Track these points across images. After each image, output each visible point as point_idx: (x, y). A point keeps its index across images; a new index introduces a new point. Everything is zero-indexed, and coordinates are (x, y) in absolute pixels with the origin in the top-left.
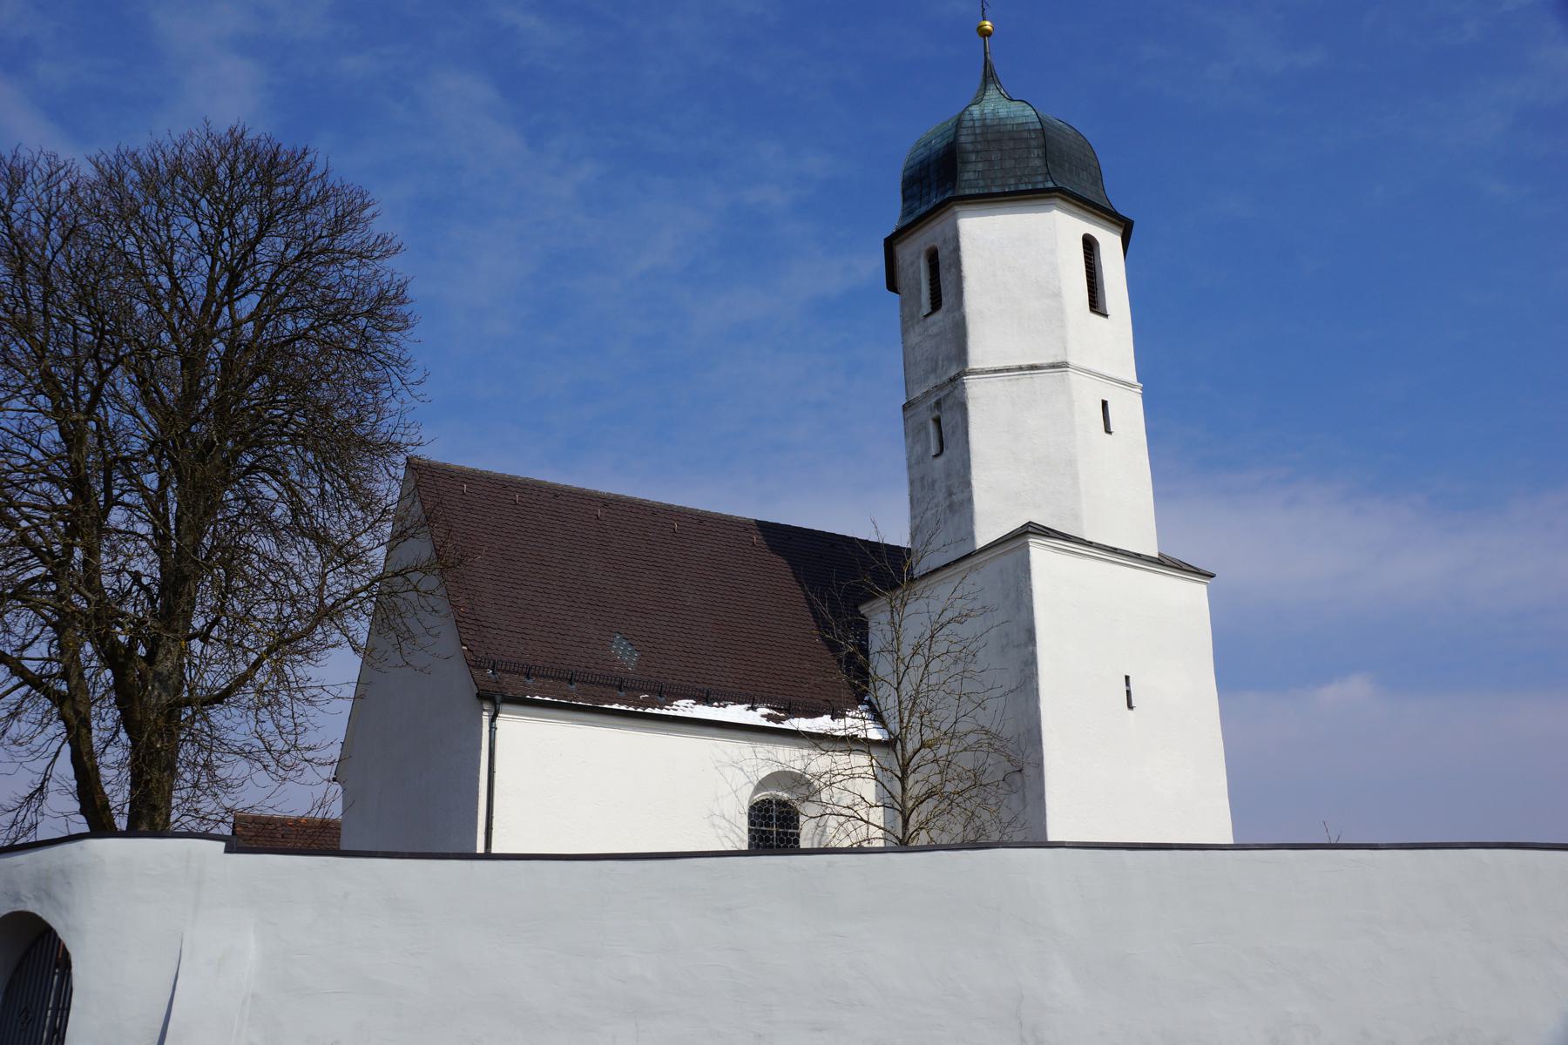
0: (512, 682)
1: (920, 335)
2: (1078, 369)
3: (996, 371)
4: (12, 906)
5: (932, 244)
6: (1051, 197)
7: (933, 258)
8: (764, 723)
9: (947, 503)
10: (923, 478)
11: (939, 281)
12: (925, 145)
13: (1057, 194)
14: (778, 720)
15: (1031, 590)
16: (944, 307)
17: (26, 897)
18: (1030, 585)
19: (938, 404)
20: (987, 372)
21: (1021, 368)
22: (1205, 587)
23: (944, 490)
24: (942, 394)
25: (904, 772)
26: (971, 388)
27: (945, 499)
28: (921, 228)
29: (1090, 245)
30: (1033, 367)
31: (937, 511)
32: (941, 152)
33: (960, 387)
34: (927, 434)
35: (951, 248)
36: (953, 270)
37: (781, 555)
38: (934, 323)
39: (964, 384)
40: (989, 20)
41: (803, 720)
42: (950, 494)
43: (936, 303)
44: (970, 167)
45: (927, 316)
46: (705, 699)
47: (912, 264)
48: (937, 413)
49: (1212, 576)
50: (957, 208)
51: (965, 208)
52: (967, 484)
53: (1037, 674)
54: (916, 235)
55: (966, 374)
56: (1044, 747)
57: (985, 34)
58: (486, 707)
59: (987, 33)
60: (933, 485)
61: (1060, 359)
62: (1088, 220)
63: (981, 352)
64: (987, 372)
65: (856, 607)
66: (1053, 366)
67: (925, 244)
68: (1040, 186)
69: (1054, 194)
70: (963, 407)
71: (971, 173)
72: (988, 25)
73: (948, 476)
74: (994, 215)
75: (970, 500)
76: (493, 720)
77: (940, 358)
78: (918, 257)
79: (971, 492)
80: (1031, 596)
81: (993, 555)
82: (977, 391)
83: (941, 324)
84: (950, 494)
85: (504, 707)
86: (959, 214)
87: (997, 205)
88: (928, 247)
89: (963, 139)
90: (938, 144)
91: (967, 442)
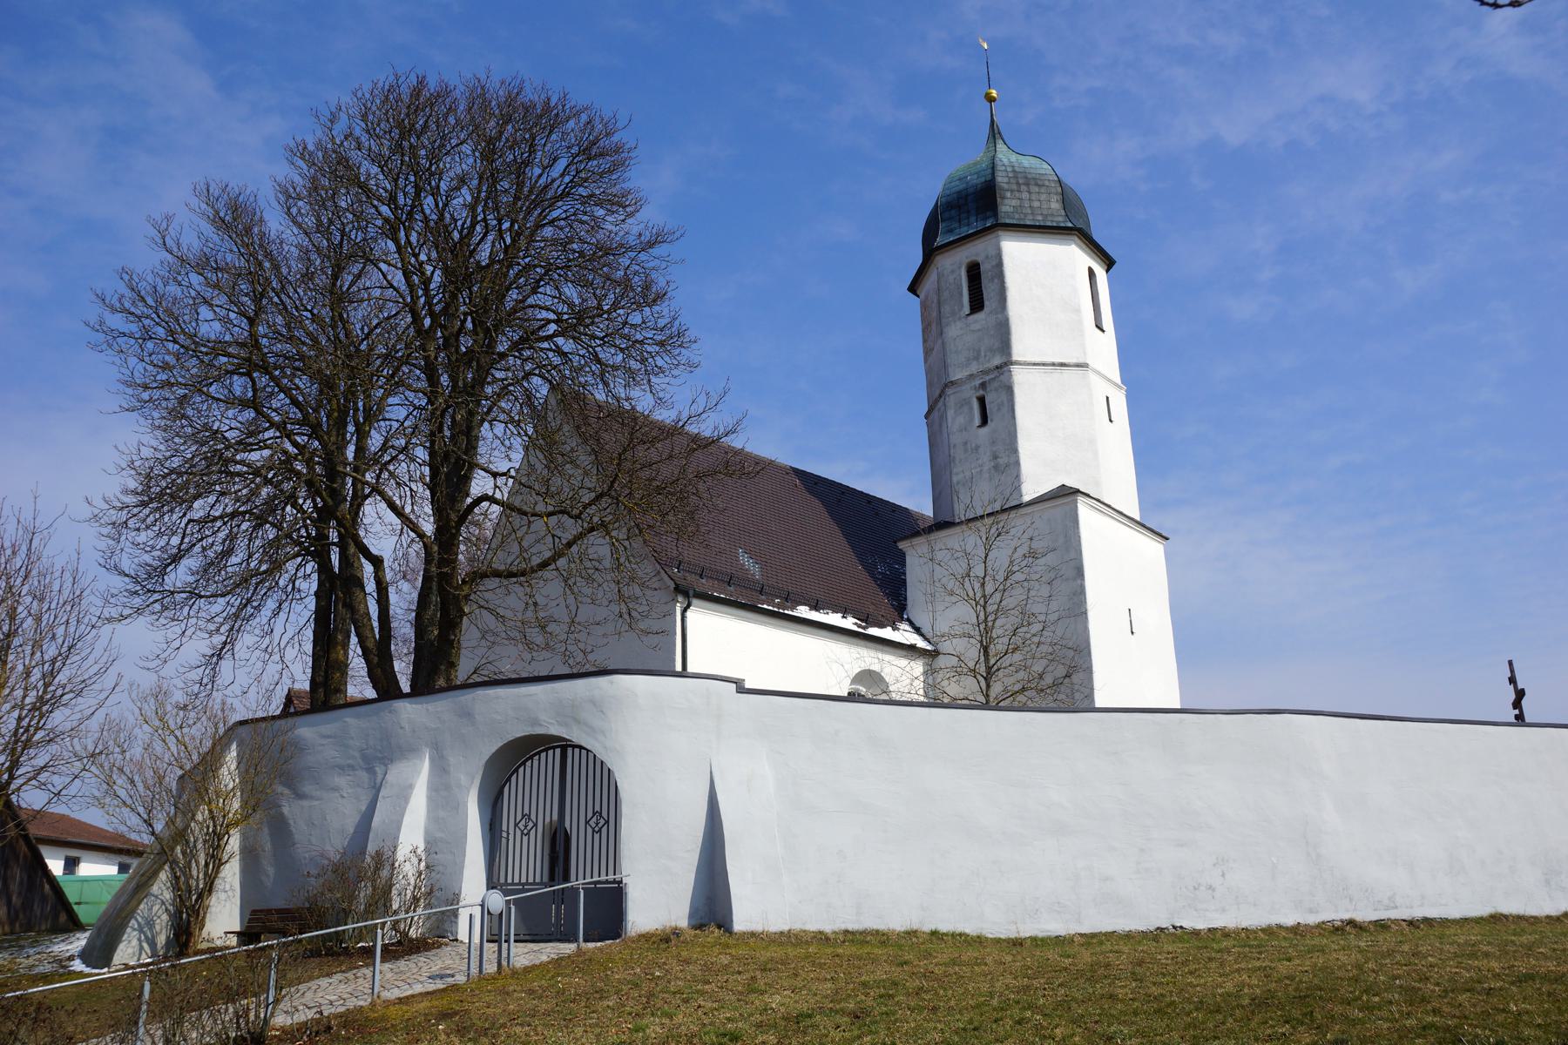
0: (704, 585)
1: (961, 329)
2: (1098, 373)
3: (1035, 364)
4: (530, 729)
5: (974, 258)
6: (1071, 234)
7: (974, 272)
8: (855, 628)
10: (966, 443)
11: (981, 287)
12: (960, 179)
13: (1076, 233)
14: (864, 628)
17: (548, 723)
18: (1078, 533)
19: (983, 385)
20: (1029, 364)
21: (1053, 364)
22: (1162, 546)
23: (988, 454)
24: (987, 378)
25: (988, 673)
29: (1091, 273)
30: (1062, 365)
31: (981, 471)
32: (979, 186)
33: (1006, 374)
34: (971, 409)
35: (994, 263)
36: (996, 281)
38: (976, 321)
41: (876, 629)
42: (995, 457)
43: (977, 304)
44: (1006, 201)
45: (968, 315)
46: (815, 607)
47: (953, 272)
48: (981, 392)
49: (1167, 539)
50: (1000, 233)
52: (1014, 450)
54: (958, 249)
55: (1012, 364)
56: (1093, 658)
57: (991, 100)
58: (680, 599)
60: (976, 450)
61: (1081, 361)
62: (1091, 257)
63: (1022, 347)
64: (1029, 364)
65: (895, 543)
66: (1078, 365)
67: (967, 258)
68: (1062, 225)
69: (1073, 232)
70: (1009, 390)
72: (994, 93)
75: (1017, 463)
76: (684, 611)
78: (960, 268)
79: (1018, 457)
80: (1080, 541)
82: (1022, 379)
83: (984, 322)
84: (995, 457)
85: (695, 601)
87: (1052, 236)
88: (969, 260)
89: (999, 179)
90: (975, 180)
91: (1014, 417)
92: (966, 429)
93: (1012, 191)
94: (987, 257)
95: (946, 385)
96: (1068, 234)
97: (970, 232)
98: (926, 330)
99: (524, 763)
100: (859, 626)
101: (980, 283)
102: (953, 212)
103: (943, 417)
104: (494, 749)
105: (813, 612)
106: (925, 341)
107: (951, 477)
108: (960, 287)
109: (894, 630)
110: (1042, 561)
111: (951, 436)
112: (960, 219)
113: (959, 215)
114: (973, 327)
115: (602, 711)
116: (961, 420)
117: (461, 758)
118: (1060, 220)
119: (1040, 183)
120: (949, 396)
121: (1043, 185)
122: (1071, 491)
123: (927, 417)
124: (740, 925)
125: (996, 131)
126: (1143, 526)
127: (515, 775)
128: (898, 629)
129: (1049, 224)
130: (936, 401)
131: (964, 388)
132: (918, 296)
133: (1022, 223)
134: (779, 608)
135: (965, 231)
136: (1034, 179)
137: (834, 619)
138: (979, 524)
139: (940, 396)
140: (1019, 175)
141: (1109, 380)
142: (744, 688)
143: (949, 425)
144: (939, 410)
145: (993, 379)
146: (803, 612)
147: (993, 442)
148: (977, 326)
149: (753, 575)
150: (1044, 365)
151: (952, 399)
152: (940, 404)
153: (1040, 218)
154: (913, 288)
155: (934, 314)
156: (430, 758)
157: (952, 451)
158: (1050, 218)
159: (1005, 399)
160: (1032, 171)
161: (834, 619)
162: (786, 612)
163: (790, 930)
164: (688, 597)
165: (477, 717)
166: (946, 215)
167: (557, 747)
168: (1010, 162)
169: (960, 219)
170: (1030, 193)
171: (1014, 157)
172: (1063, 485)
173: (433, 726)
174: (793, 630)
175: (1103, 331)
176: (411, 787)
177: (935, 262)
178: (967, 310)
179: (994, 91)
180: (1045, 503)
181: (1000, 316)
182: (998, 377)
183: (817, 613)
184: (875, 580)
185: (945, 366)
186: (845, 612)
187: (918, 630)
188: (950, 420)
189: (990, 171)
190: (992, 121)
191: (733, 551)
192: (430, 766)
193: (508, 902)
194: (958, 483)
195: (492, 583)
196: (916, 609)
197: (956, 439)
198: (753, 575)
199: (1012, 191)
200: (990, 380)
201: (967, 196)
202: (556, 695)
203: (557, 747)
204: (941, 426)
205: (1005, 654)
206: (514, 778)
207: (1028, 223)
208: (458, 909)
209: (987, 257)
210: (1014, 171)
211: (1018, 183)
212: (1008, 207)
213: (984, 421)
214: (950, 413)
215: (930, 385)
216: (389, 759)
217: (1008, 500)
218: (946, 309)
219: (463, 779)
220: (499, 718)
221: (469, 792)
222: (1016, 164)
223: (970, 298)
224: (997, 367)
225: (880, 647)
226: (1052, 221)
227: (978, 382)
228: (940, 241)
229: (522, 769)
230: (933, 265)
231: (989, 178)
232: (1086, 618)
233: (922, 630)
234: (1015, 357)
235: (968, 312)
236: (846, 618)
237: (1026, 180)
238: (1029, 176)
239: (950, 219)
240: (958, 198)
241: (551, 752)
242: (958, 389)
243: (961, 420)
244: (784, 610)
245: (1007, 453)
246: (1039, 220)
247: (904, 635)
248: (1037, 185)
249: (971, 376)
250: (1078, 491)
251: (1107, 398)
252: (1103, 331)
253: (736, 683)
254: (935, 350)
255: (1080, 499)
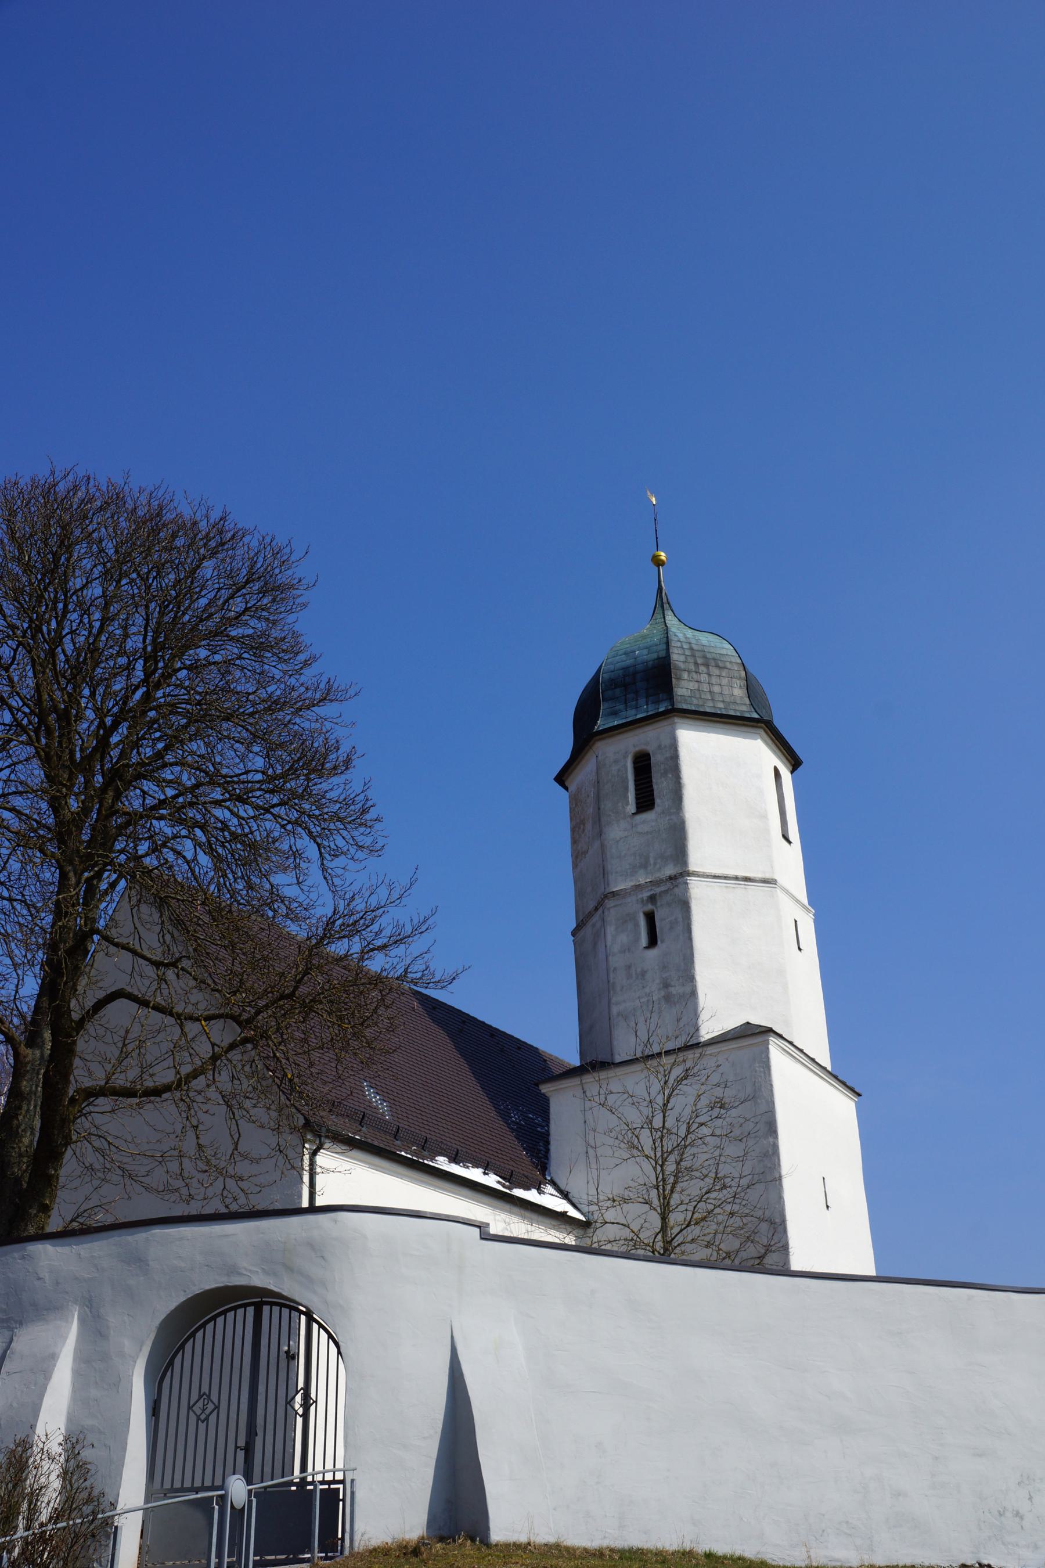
0: (334, 1122)
2: (786, 892)
6: (757, 727)
7: (643, 764)
8: (500, 1187)
9: (663, 993)
10: (629, 967)
12: (626, 654)
13: (763, 725)
14: (510, 1189)
15: (771, 1085)
16: (658, 808)
17: (250, 1271)
19: (652, 899)
20: (708, 876)
21: (736, 878)
23: (657, 981)
24: (658, 890)
26: (694, 888)
27: (659, 989)
28: (631, 730)
30: (747, 879)
32: (651, 663)
34: (637, 925)
37: (442, 1027)
38: (644, 822)
39: (687, 883)
40: (662, 551)
41: (522, 1190)
42: (666, 985)
43: (645, 801)
44: (683, 684)
46: (454, 1159)
47: (616, 761)
48: (649, 907)
50: (677, 720)
51: (686, 721)
53: (779, 1165)
57: (658, 563)
59: (661, 563)
61: (768, 876)
64: (708, 876)
65: (537, 1085)
66: (765, 881)
67: (634, 746)
68: (747, 715)
69: (759, 725)
70: (685, 906)
71: (684, 690)
72: (663, 556)
73: (664, 968)
74: (709, 733)
75: (694, 993)
76: (314, 1154)
77: (652, 855)
78: (625, 757)
81: (726, 1048)
82: (698, 891)
84: (666, 985)
86: (678, 725)
88: (637, 749)
90: (644, 656)
91: (690, 938)
92: (629, 950)
93: (689, 672)
94: (659, 747)
95: (606, 896)
96: (753, 726)
97: (639, 716)
98: (577, 828)
99: (203, 1326)
100: (504, 1186)
101: (651, 777)
102: (618, 690)
103: (599, 935)
104: (173, 1305)
105: (453, 1165)
106: (574, 842)
107: (609, 1007)
108: (625, 781)
109: (540, 1194)
110: (734, 1112)
111: (610, 958)
112: (626, 700)
113: (625, 695)
114: (641, 829)
115: (323, 1257)
116: (624, 938)
117: (126, 1318)
118: (744, 708)
119: (721, 664)
120: (609, 909)
121: (725, 668)
122: (764, 1029)
123: (574, 933)
124: (498, 1533)
125: (665, 600)
126: (836, 1077)
127: (192, 1340)
128: (544, 1193)
129: (732, 713)
130: (590, 915)
131: (629, 900)
132: (566, 789)
133: (701, 710)
134: (412, 1156)
135: (632, 715)
136: (714, 659)
137: (475, 1174)
138: (654, 1062)
139: (596, 909)
140: (697, 654)
141: (798, 901)
142: (489, 1234)
143: (609, 944)
144: (594, 925)
145: (666, 892)
146: (442, 1163)
147: (664, 967)
148: (645, 828)
149: (383, 1114)
150: (726, 878)
151: (613, 912)
152: (596, 918)
153: (721, 705)
154: (561, 779)
155: (590, 811)
156: (79, 1319)
157: (612, 975)
158: (732, 707)
159: (680, 916)
160: (712, 650)
161: (475, 1174)
162: (426, 1162)
163: (529, 1544)
164: (320, 1137)
165: (151, 1263)
166: (609, 693)
167: (249, 1304)
168: (686, 638)
169: (626, 700)
170: (709, 675)
171: (689, 633)
172: (748, 1023)
173: (86, 1276)
174: (432, 1185)
175: (790, 842)
176: (53, 1357)
177: (594, 748)
178: (632, 808)
179: (663, 554)
180: (731, 1042)
181: (673, 817)
182: (671, 889)
183: (458, 1166)
184: (512, 1130)
185: (605, 873)
186: (487, 1169)
187: (565, 1195)
188: (609, 938)
189: (664, 647)
190: (660, 589)
191: (358, 1083)
192: (79, 1328)
193: (250, 1491)
194: (619, 1014)
195: (103, 1103)
196: (557, 1169)
197: (617, 961)
198: (383, 1114)
199: (689, 672)
200: (661, 893)
201: (635, 673)
202: (262, 1235)
203: (249, 1304)
204: (595, 944)
205: (688, 1226)
206: (189, 1346)
207: (708, 710)
208: (113, 1516)
209: (659, 747)
210: (691, 649)
211: (696, 664)
212: (684, 689)
213: (653, 941)
214: (610, 930)
215: (580, 895)
216: (16, 1322)
217: (692, 1037)
218: (607, 805)
219: (128, 1345)
220: (183, 1265)
221: (135, 1362)
222: (693, 641)
223: (636, 794)
224: (670, 878)
225: (534, 1216)
226: (735, 710)
227: (646, 894)
228: (601, 724)
229: (200, 1334)
230: (590, 753)
231: (663, 654)
232: (781, 1185)
233: (570, 1196)
234: (693, 867)
235: (634, 810)
236: (487, 1174)
237: (707, 661)
238: (709, 656)
239: (612, 699)
240: (624, 676)
241: (240, 1312)
242: (619, 902)
243: (624, 938)
244: (423, 1160)
245: (681, 981)
246: (720, 709)
247: (551, 1200)
248: (717, 666)
249: (638, 887)
250: (770, 1031)
251: (796, 921)
252: (790, 842)
253: (479, 1227)
254: (590, 852)
255: (773, 1040)
